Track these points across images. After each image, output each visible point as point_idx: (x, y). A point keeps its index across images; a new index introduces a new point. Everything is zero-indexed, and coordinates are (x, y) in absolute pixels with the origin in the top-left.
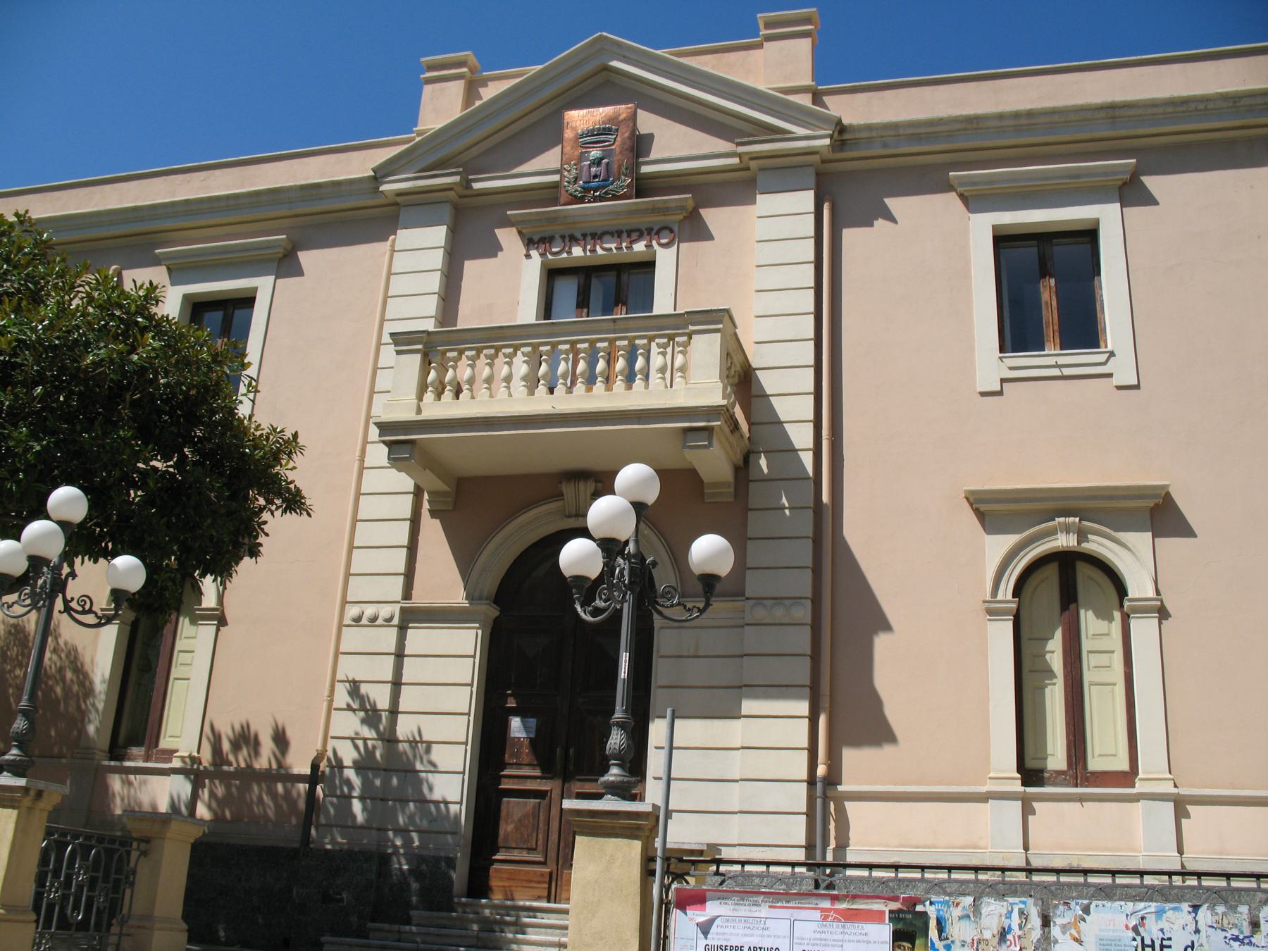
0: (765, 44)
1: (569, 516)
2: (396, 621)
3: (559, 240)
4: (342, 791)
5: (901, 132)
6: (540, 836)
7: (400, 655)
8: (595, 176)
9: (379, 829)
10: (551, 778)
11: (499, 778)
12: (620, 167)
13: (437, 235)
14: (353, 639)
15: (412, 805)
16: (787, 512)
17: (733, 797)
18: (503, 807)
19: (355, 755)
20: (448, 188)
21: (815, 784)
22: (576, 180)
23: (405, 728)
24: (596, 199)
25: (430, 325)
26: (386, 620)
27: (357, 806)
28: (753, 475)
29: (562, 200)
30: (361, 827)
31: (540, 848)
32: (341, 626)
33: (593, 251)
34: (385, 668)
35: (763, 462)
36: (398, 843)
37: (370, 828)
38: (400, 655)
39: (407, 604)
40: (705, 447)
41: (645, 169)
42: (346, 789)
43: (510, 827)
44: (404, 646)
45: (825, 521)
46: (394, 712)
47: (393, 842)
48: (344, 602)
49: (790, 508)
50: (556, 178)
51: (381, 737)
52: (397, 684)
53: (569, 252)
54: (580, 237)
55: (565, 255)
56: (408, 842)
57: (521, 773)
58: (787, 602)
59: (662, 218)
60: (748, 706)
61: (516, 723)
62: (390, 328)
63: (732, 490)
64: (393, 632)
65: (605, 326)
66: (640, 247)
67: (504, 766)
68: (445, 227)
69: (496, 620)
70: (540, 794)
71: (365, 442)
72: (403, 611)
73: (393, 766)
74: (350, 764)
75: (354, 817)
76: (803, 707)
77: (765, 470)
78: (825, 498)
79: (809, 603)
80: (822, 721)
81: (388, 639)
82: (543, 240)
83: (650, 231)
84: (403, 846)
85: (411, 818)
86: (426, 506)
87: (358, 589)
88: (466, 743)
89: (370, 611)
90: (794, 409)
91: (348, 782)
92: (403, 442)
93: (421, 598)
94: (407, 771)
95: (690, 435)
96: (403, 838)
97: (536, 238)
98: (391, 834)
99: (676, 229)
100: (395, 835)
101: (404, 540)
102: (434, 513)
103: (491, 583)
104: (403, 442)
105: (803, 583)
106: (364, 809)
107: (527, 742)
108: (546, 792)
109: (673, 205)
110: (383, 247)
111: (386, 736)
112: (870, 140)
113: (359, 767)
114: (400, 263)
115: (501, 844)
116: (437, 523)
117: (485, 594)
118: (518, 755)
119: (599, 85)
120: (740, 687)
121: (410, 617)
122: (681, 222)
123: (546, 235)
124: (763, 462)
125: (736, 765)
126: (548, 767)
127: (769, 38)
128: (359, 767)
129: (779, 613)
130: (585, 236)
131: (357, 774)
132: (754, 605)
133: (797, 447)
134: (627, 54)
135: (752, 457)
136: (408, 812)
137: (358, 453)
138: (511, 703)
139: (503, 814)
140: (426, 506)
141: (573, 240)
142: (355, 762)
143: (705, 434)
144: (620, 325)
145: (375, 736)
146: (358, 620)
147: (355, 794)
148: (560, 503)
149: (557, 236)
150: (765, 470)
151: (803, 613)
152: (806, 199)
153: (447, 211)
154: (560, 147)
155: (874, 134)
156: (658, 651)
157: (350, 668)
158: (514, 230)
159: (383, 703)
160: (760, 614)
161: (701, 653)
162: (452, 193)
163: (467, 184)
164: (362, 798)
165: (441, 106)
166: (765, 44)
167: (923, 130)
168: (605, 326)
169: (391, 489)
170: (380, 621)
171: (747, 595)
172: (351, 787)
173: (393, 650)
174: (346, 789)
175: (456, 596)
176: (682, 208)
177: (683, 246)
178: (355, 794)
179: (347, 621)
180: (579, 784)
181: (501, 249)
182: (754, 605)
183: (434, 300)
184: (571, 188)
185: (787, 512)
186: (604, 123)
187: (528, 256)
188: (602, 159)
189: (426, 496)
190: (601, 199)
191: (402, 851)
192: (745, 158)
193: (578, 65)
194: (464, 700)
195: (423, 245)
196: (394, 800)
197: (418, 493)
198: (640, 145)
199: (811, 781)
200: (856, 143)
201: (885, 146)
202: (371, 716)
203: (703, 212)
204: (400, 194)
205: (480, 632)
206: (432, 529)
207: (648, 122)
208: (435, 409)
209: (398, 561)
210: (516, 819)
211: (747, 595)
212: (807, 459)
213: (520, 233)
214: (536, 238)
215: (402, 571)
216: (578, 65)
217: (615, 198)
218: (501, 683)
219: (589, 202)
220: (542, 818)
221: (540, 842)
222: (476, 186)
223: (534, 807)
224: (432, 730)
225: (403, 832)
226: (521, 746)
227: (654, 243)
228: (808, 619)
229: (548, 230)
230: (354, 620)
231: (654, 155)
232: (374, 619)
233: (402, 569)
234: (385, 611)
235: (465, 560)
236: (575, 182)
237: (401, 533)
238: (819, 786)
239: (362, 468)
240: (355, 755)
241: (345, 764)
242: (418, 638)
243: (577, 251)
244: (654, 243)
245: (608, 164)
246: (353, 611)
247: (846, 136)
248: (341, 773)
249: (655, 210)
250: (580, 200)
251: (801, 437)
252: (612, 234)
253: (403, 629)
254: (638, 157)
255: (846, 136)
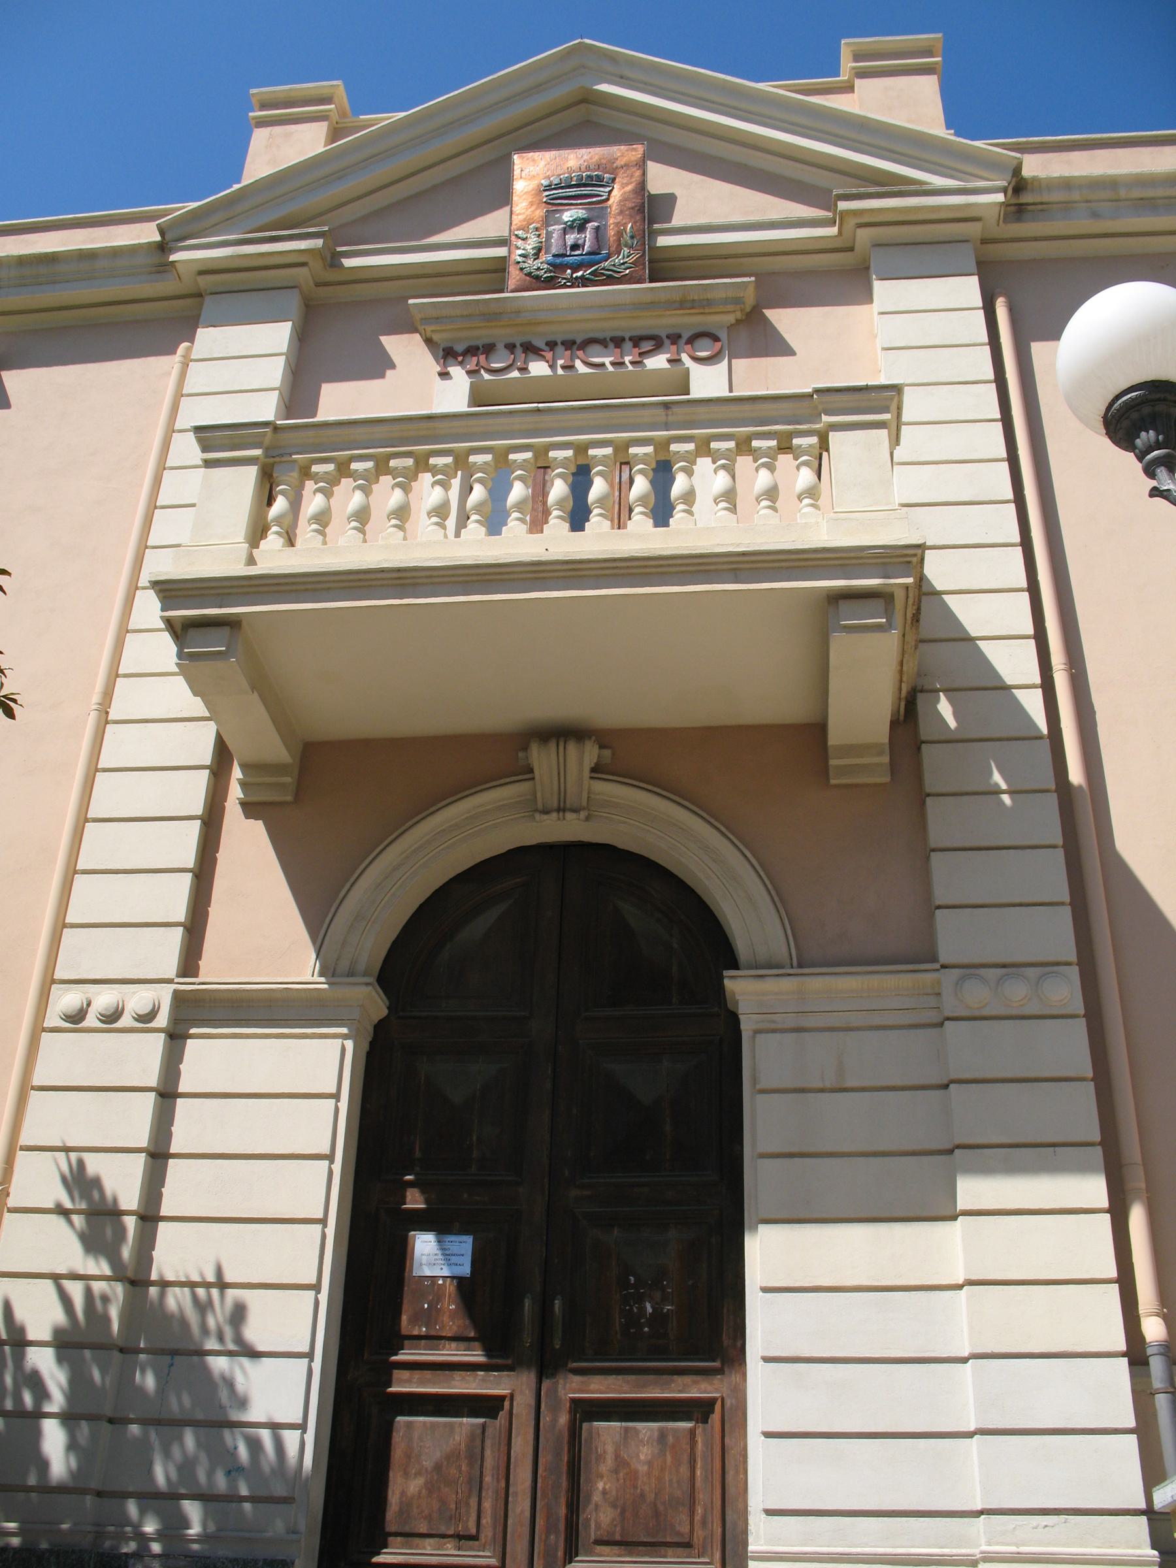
0: (858, 83)
1: (546, 812)
2: (162, 1020)
3: (501, 351)
4: (18, 1399)
5: (1123, 193)
6: (487, 1505)
7: (167, 1094)
8: (575, 247)
9: (99, 1494)
10: (511, 1368)
11: (386, 1371)
12: (620, 234)
13: (277, 336)
14: (62, 1058)
15: (189, 1439)
16: (1006, 799)
17: (963, 1397)
18: (398, 1437)
19: (58, 1316)
20: (297, 262)
21: (1146, 1363)
22: (538, 251)
23: (177, 1255)
24: (574, 283)
25: (266, 409)
26: (141, 1018)
27: (54, 1440)
28: (926, 730)
29: (512, 283)
30: (61, 1489)
31: (487, 1533)
32: (38, 1029)
33: (569, 367)
34: (135, 1120)
35: (945, 707)
36: (149, 1528)
37: (83, 1491)
38: (167, 1094)
39: (188, 985)
40: (878, 628)
41: (663, 241)
42: (28, 1399)
43: (415, 1485)
44: (178, 1074)
45: (1079, 819)
46: (150, 1217)
47: (137, 1527)
48: (49, 981)
49: (1010, 792)
50: (501, 252)
51: (119, 1275)
52: (158, 1155)
53: (524, 370)
54: (543, 346)
55: (515, 374)
56: (174, 1525)
57: (439, 1357)
58: (1031, 972)
59: (699, 319)
60: (972, 1190)
61: (424, 1245)
62: (161, 566)
63: (886, 759)
64: (156, 1044)
65: (647, 415)
66: (658, 362)
67: (397, 1341)
68: (290, 323)
69: (380, 1028)
70: (487, 1406)
71: (124, 630)
72: (179, 999)
73: (145, 1349)
74: (47, 1336)
75: (43, 1465)
76: (1093, 1189)
77: (952, 723)
78: (1076, 775)
79: (1074, 972)
80: (1137, 1219)
81: (144, 1056)
82: (472, 351)
83: (675, 339)
84: (160, 1536)
85: (186, 1468)
86: (235, 792)
87: (81, 954)
88: (317, 1288)
89: (104, 999)
90: (992, 613)
91: (35, 1381)
92: (205, 620)
93: (219, 971)
94: (174, 1353)
95: (844, 606)
96: (161, 1515)
97: (460, 348)
98: (132, 1508)
99: (723, 335)
100: (143, 1512)
101: (189, 859)
102: (250, 809)
103: (373, 945)
104: (205, 620)
105: (1055, 935)
106: (72, 1445)
107: (451, 1287)
108: (502, 1398)
109: (721, 294)
110: (168, 365)
111: (130, 1274)
112: (1067, 207)
113: (66, 1344)
114: (198, 377)
115: (391, 1527)
116: (257, 829)
117: (361, 966)
118: (429, 1317)
119: (577, 118)
120: (950, 1152)
121: (196, 1012)
122: (730, 328)
123: (480, 343)
124: (945, 707)
125: (959, 1323)
126: (500, 1343)
127: (863, 74)
128: (66, 1344)
129: (1017, 993)
130: (552, 345)
131: (60, 1359)
132: (962, 979)
133: (1009, 681)
134: (627, 72)
135: (921, 698)
136: (176, 1451)
137: (96, 698)
138: (415, 1201)
139: (398, 1452)
140: (235, 792)
141: (531, 350)
142: (58, 1332)
143: (879, 604)
144: (679, 413)
145: (107, 1271)
146: (76, 1018)
147: (50, 1408)
148: (523, 788)
149: (500, 346)
150: (952, 723)
151: (1066, 992)
152: (968, 289)
153: (293, 301)
154: (507, 209)
155: (1076, 196)
156: (755, 1080)
157: (49, 1120)
158: (417, 336)
159: (128, 1195)
160: (977, 995)
161: (850, 1083)
162: (304, 271)
163: (333, 260)
164: (68, 1418)
165: (280, 149)
166: (858, 83)
167: (1160, 192)
168: (647, 415)
169: (167, 725)
170: (126, 1021)
171: (944, 958)
172: (41, 1393)
173: (153, 1081)
174: (28, 1399)
175: (297, 965)
176: (737, 301)
177: (740, 364)
178: (50, 1408)
179: (53, 1019)
180: (577, 1379)
181: (392, 366)
182: (962, 979)
183: (281, 362)
184: (532, 265)
185: (1006, 799)
186: (588, 169)
187: (444, 375)
188: (586, 221)
189: (237, 773)
190: (584, 282)
191: (156, 1548)
192: (851, 222)
193: (538, 88)
194: (314, 1191)
195: (241, 365)
196: (143, 1422)
197: (222, 756)
198: (652, 209)
199: (1136, 1353)
200: (1043, 210)
201: (1095, 215)
202: (97, 1219)
203: (771, 314)
204: (207, 270)
205: (349, 1044)
206: (248, 844)
207: (662, 178)
208: (275, 557)
209: (175, 898)
210: (428, 1464)
211: (944, 958)
212: (1033, 703)
213: (429, 342)
214: (460, 348)
215: (191, 865)
216: (538, 88)
217: (610, 280)
218: (398, 1154)
219: (565, 286)
220: (489, 1462)
221: (487, 1520)
222: (348, 263)
223: (471, 1438)
224: (248, 1256)
225: (164, 1502)
226: (439, 1298)
227: (685, 357)
228: (1079, 1007)
229: (482, 335)
230: (69, 1018)
231: (677, 221)
232: (112, 1017)
233: (180, 914)
234: (138, 1000)
235: (318, 901)
236: (537, 256)
237: (183, 844)
238: (1157, 1365)
239: (104, 720)
240: (58, 1316)
241: (31, 1336)
242: (210, 1058)
243: (538, 368)
244: (685, 357)
245: (597, 229)
246: (66, 1000)
247: (1026, 198)
248: (19, 1358)
249: (684, 303)
250: (550, 283)
251: (1015, 664)
252: (602, 342)
253: (176, 1037)
254: (651, 223)
255: (1026, 198)
